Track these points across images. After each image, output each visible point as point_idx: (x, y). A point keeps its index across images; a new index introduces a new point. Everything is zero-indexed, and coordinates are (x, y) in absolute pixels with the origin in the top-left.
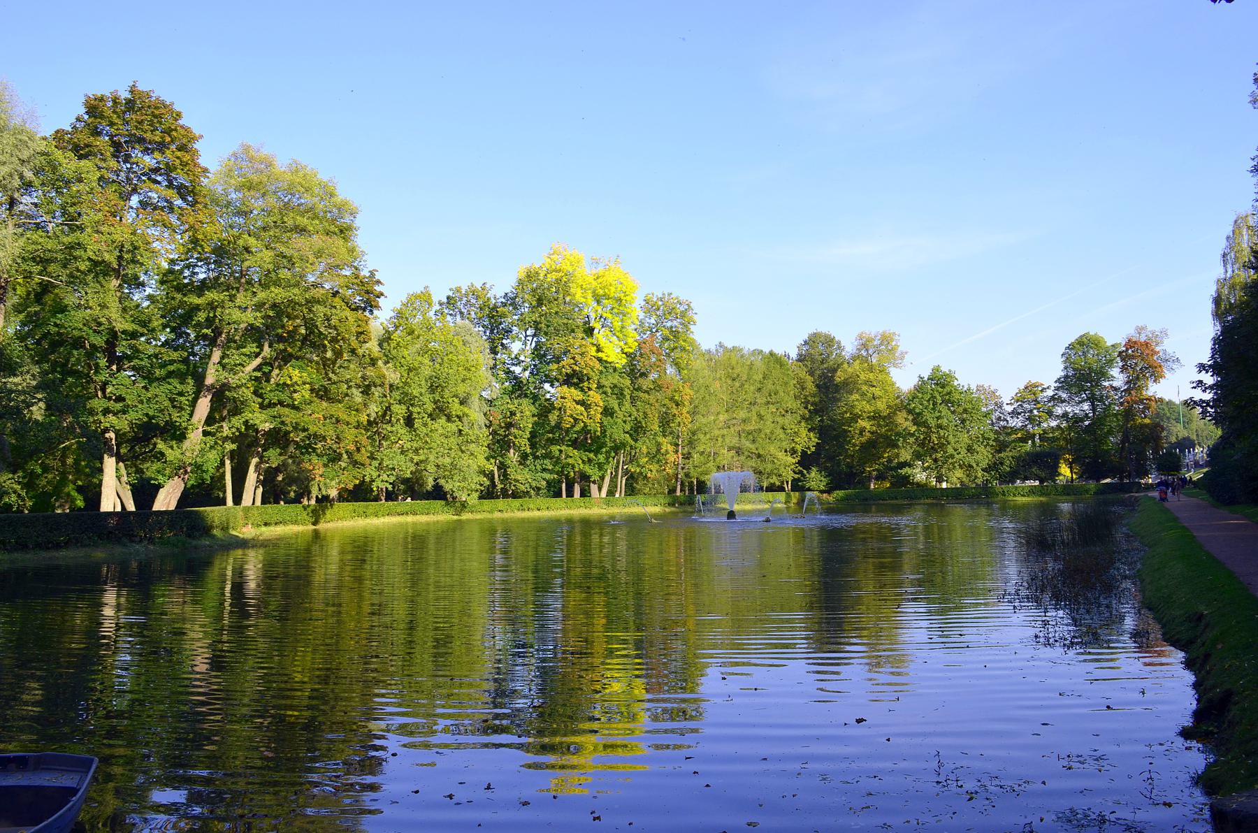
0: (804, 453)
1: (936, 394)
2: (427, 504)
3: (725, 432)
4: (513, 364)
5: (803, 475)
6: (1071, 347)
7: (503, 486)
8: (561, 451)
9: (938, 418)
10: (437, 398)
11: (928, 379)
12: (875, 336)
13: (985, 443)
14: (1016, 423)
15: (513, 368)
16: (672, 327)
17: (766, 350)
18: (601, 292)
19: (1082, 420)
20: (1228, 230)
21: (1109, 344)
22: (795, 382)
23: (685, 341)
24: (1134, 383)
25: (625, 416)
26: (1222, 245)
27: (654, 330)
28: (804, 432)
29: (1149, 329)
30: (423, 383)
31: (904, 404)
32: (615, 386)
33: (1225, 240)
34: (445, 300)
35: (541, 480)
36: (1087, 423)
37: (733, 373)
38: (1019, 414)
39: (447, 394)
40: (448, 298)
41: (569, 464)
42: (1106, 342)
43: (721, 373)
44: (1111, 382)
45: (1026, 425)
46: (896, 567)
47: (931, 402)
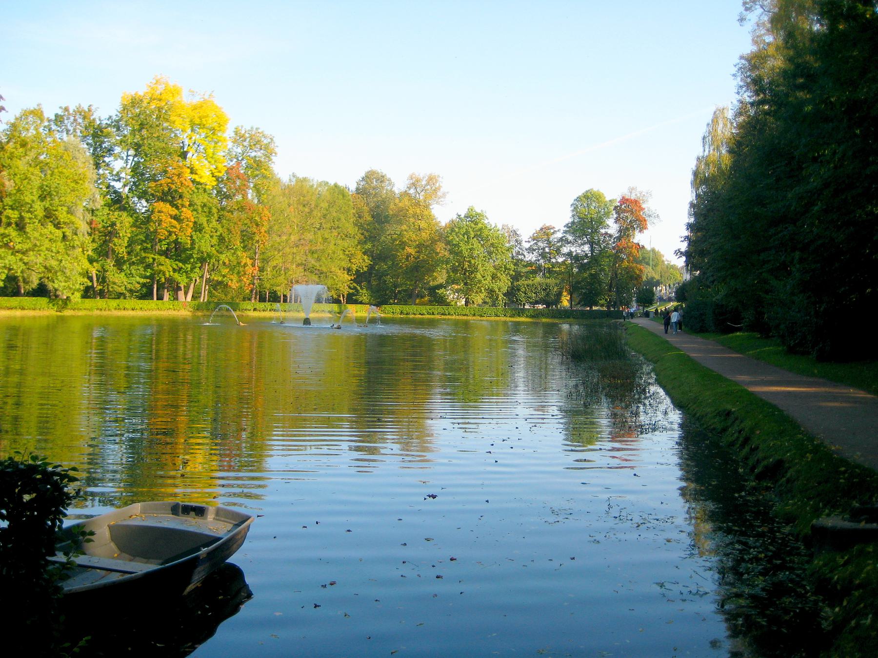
0: (357, 271)
1: (470, 230)
2: (34, 300)
3: (295, 250)
4: (114, 180)
5: (357, 291)
6: (578, 199)
7: (101, 287)
8: (154, 259)
9: (471, 249)
10: (47, 206)
11: (465, 217)
12: (423, 178)
13: (506, 273)
14: (531, 257)
15: (113, 183)
16: (255, 157)
17: (332, 183)
18: (197, 121)
19: (583, 259)
20: (709, 118)
21: (607, 199)
22: (354, 211)
23: (266, 170)
24: (625, 232)
25: (212, 232)
26: (703, 130)
27: (240, 159)
28: (359, 255)
29: (639, 189)
30: (35, 191)
31: (445, 236)
32: (205, 205)
33: (706, 126)
34: (53, 118)
35: (137, 281)
36: (585, 261)
37: (304, 200)
38: (535, 250)
39: (56, 201)
40: (57, 115)
41: (161, 271)
42: (605, 198)
43: (293, 200)
44: (607, 230)
45: (539, 260)
46: (429, 366)
47: (466, 236)
